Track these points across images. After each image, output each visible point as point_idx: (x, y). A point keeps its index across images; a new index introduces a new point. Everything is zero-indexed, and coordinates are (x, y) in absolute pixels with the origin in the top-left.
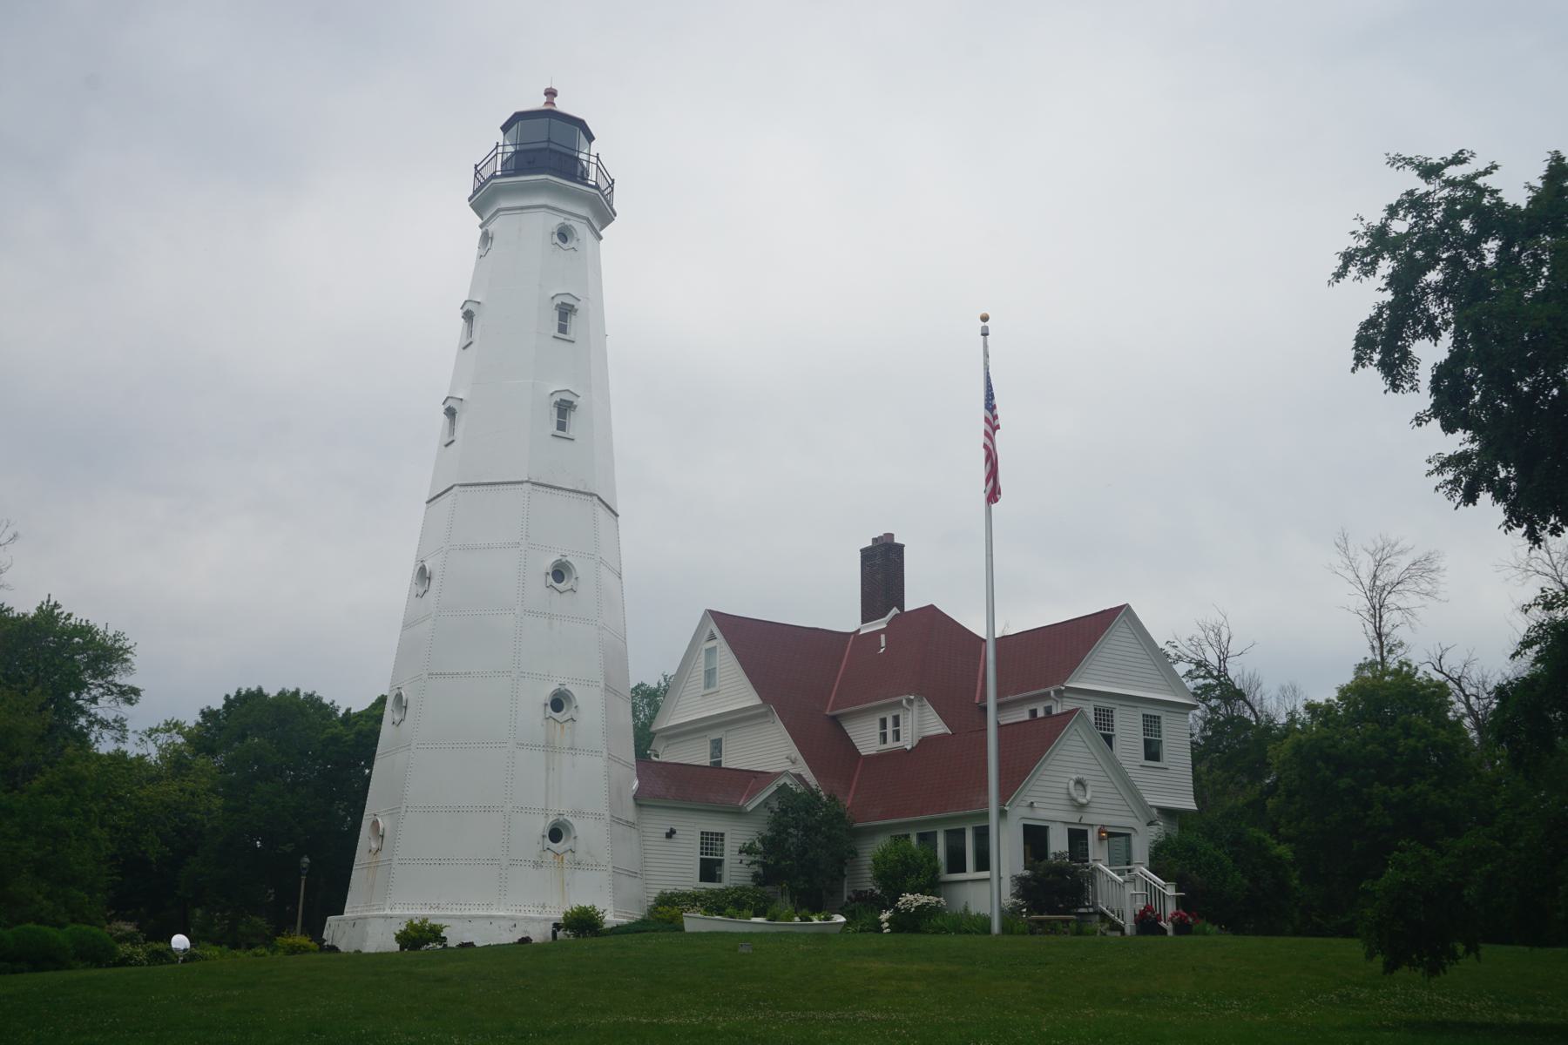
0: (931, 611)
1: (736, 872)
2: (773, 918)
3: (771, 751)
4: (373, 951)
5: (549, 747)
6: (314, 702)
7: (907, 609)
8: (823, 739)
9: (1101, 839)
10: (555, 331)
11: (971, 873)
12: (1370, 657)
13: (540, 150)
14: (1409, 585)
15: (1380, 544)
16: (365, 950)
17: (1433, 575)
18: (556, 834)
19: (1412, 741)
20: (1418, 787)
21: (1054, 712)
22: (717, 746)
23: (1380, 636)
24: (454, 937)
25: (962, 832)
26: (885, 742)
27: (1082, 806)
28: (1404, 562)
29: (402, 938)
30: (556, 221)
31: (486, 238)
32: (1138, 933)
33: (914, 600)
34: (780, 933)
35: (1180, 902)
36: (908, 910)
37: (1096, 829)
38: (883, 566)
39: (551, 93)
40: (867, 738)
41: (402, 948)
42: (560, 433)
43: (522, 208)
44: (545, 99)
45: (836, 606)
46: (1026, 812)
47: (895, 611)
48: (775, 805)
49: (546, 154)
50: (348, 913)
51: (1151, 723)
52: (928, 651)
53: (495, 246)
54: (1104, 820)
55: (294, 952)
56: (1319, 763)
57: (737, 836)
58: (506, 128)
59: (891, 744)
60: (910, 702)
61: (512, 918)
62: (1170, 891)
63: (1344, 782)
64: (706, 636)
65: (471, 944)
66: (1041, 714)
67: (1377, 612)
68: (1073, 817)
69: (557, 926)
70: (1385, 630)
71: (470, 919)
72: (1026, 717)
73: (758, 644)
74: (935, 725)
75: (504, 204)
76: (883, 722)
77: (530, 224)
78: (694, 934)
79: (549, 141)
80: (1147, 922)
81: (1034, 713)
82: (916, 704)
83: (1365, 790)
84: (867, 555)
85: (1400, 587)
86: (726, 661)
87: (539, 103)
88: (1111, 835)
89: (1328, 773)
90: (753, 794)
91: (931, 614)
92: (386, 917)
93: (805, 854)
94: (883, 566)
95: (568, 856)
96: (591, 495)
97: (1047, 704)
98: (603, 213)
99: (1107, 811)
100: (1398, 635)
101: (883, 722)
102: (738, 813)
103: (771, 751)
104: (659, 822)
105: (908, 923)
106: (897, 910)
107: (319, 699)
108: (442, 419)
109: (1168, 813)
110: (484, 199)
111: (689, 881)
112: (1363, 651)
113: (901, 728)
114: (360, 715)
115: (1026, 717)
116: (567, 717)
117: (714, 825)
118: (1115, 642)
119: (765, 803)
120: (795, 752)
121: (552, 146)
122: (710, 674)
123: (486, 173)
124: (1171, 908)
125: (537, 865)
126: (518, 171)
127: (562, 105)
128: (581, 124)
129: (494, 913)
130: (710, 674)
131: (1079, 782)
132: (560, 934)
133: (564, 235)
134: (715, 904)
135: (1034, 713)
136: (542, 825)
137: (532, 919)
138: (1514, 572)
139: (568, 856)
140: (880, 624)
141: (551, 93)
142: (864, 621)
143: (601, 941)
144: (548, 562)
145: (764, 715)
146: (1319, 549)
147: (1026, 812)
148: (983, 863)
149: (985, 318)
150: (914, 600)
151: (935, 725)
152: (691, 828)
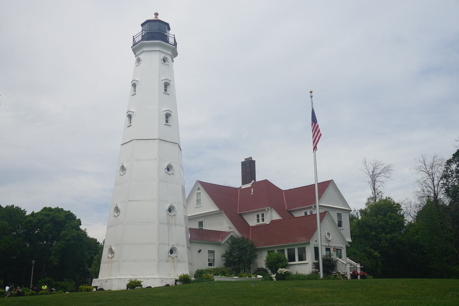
0: (266, 181)
1: (219, 263)
2: (241, 277)
3: (224, 225)
4: (116, 290)
5: (169, 224)
6: (18, 209)
7: (256, 181)
8: (238, 221)
9: (334, 251)
10: (163, 91)
11: (297, 262)
12: (372, 196)
13: (157, 32)
14: (382, 174)
15: (375, 162)
16: (113, 290)
17: (390, 172)
18: (171, 252)
19: (392, 221)
20: (395, 235)
21: (313, 213)
22: (201, 224)
23: (374, 189)
24: (145, 284)
25: (283, 251)
26: (258, 221)
27: (329, 241)
28: (382, 167)
29: (128, 286)
30: (162, 56)
31: (139, 60)
32: (352, 278)
33: (259, 177)
34: (242, 281)
35: (361, 269)
36: (281, 274)
37: (333, 248)
38: (249, 168)
39: (156, 14)
40: (252, 221)
41: (127, 288)
42: (167, 124)
43: (151, 51)
44: (154, 16)
45: (234, 180)
46: (315, 243)
47: (253, 181)
48: (230, 242)
49: (156, 33)
50: (99, 279)
51: (339, 215)
52: (268, 193)
53: (142, 63)
54: (335, 245)
55: (88, 291)
56: (365, 228)
57: (219, 253)
58: (142, 25)
59: (261, 222)
60: (268, 209)
61: (161, 279)
62: (359, 266)
63: (373, 233)
64: (197, 188)
65: (151, 287)
66: (309, 214)
67: (374, 182)
68: (327, 244)
69: (176, 281)
70: (376, 188)
71: (148, 279)
72: (304, 215)
73: (217, 192)
74: (276, 216)
75: (145, 49)
76: (258, 216)
77: (153, 57)
78: (217, 282)
79: (160, 30)
80: (354, 276)
81: (306, 214)
82: (270, 210)
83: (380, 235)
84: (243, 164)
85: (380, 175)
86: (205, 197)
87: (152, 17)
88: (337, 249)
89: (368, 231)
90: (223, 238)
91: (266, 183)
92: (119, 279)
93: (239, 257)
94: (249, 168)
95: (175, 258)
96: (176, 143)
97: (311, 210)
98: (175, 54)
99: (336, 242)
100: (380, 189)
101: (258, 216)
102: (219, 244)
103: (224, 225)
104: (196, 247)
105: (281, 277)
106: (277, 274)
107: (20, 208)
108: (125, 118)
109: (348, 242)
110: (136, 48)
111: (205, 266)
112: (369, 193)
113: (265, 217)
114: (38, 213)
115: (304, 215)
116: (173, 214)
117: (212, 248)
118: (329, 191)
119: (227, 241)
120: (231, 225)
121: (161, 32)
122: (198, 201)
123: (137, 40)
124: (359, 271)
125: (167, 261)
126: (148, 39)
127: (160, 18)
128: (167, 25)
129: (155, 277)
130: (198, 201)
131: (328, 234)
132: (178, 283)
133: (164, 60)
134: (217, 272)
135: (306, 214)
136: (168, 249)
137: (168, 279)
138: (414, 170)
139: (175, 258)
140: (249, 185)
141: (156, 14)
142: (242, 184)
143: (191, 285)
144: (165, 165)
145: (220, 213)
146: (377, 164)
147: (315, 243)
148: (302, 258)
149: (311, 92)
150: (259, 177)
151: (276, 216)
152: (206, 249)
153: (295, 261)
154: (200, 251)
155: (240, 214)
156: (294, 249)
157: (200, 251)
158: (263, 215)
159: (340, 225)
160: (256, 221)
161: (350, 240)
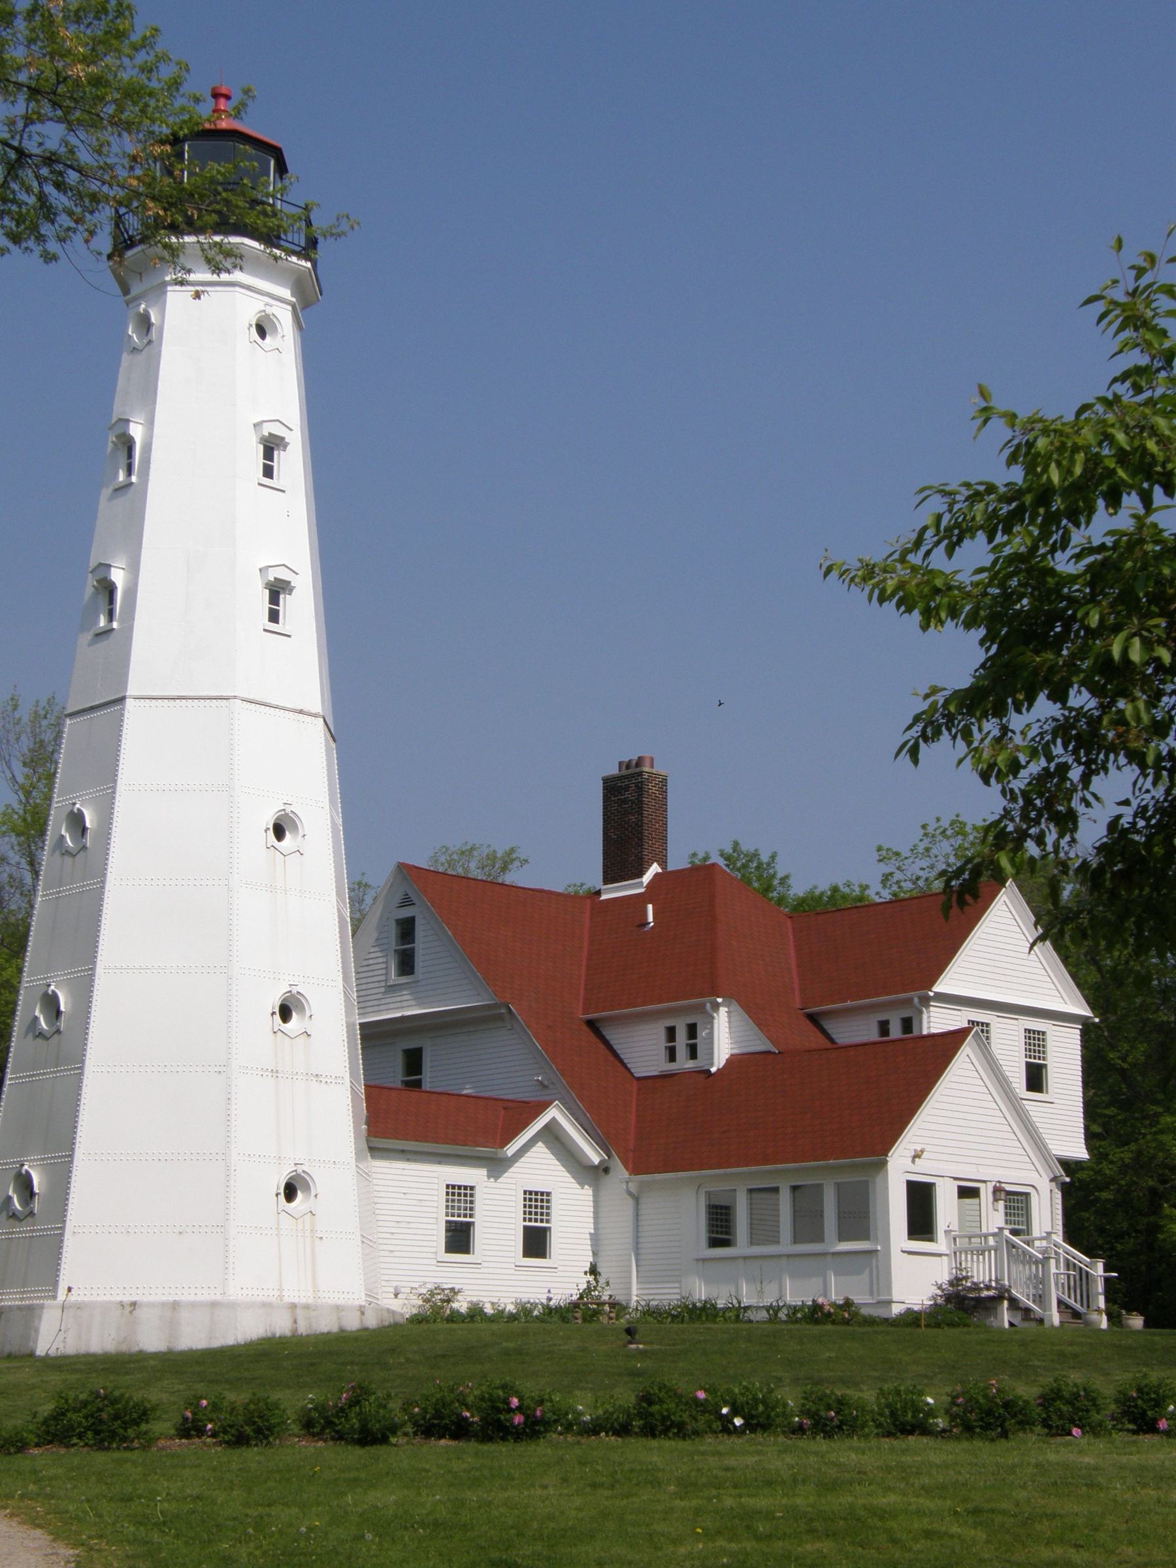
37: (990, 1187)
38: (630, 812)
45: (564, 855)
47: (655, 869)
51: (1035, 1040)
59: (684, 1063)
66: (896, 1032)
72: (873, 1035)
76: (671, 1033)
81: (884, 1028)
94: (630, 812)
101: (671, 1033)
115: (873, 1035)
135: (884, 1028)
142: (607, 880)
153: (778, 1242)
154: (938, 820)
155: (591, 1024)
156: (819, 1187)
157: (938, 820)
158: (692, 1031)
159: (1036, 1079)
160: (663, 1054)
161: (1079, 1151)
